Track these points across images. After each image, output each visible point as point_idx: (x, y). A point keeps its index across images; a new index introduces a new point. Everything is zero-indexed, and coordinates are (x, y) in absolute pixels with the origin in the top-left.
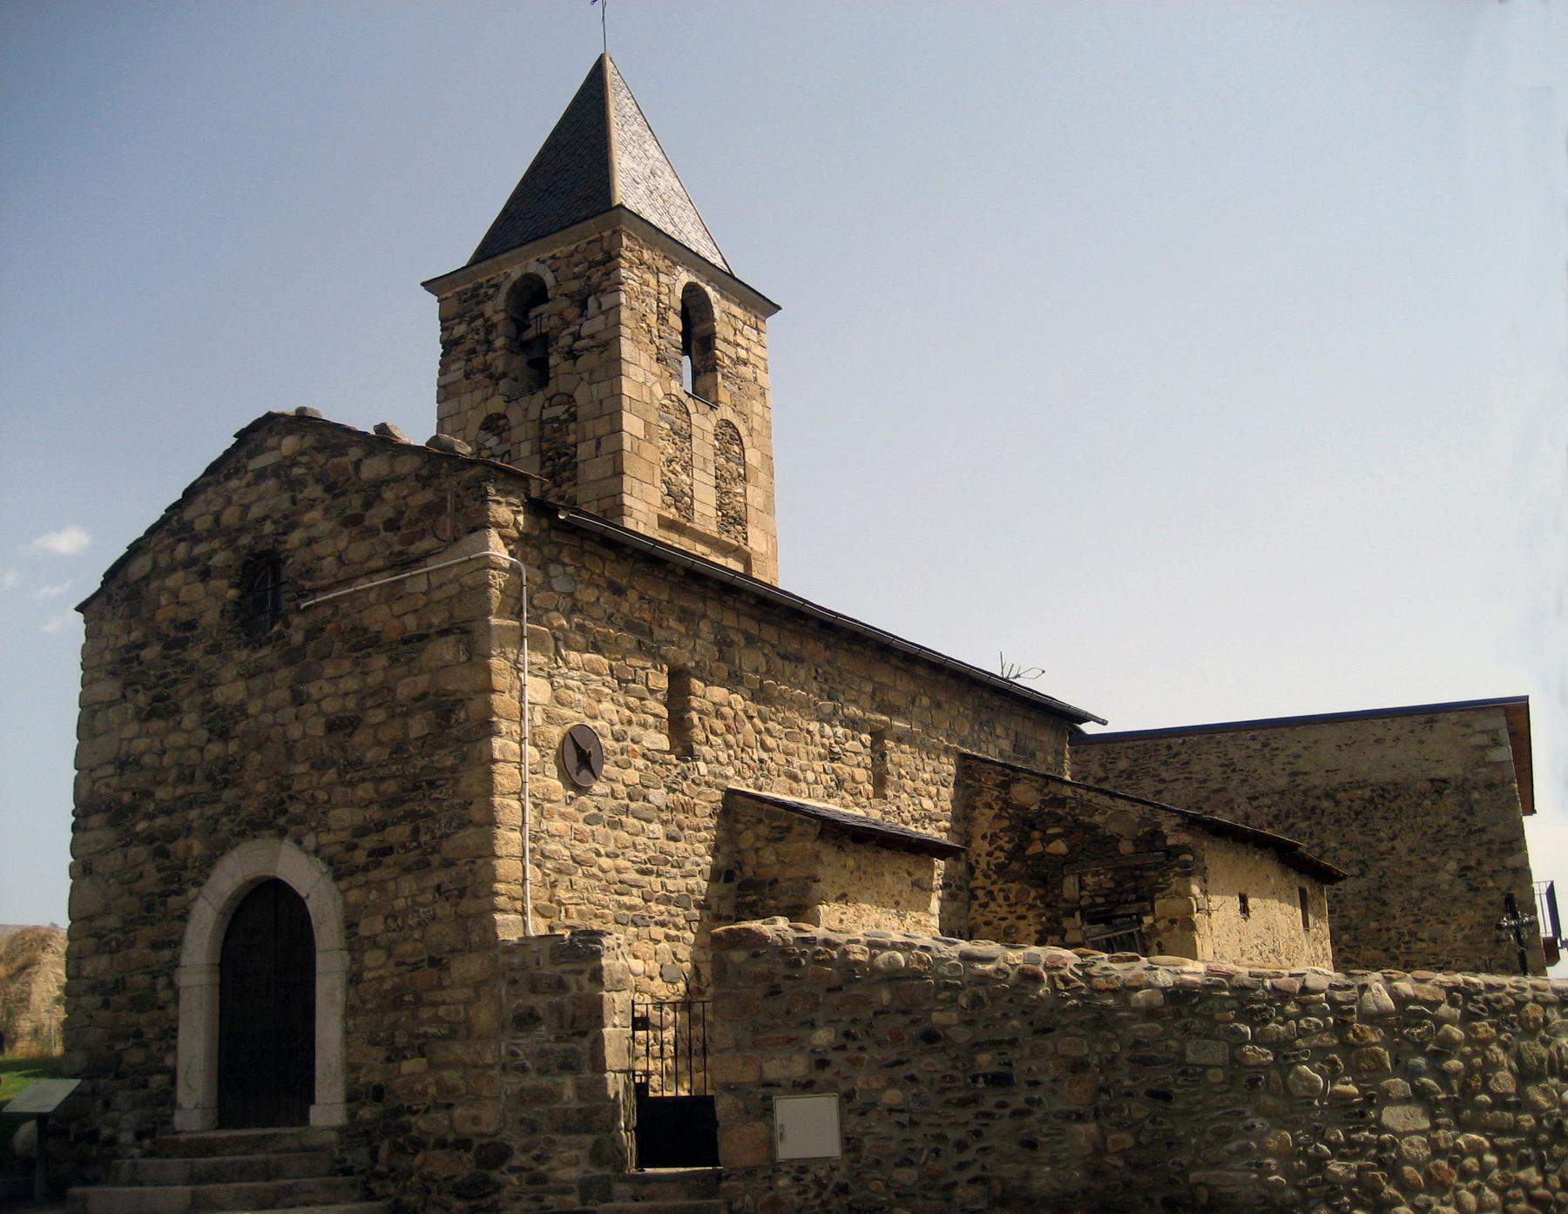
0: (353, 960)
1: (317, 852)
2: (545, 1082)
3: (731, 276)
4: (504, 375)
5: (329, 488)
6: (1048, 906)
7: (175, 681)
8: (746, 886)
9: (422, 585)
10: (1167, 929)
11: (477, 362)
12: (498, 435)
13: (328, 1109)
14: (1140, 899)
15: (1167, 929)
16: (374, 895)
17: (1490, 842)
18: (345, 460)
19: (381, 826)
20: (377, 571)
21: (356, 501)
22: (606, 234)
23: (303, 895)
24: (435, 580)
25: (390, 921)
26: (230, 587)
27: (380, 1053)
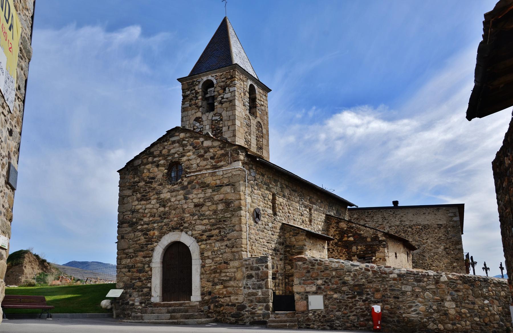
0: (203, 262)
1: (192, 236)
2: (254, 291)
3: (259, 81)
4: (201, 106)
5: (194, 148)
6: (348, 253)
7: (149, 192)
8: (287, 246)
9: (221, 173)
10: (379, 261)
11: (193, 102)
12: (200, 123)
13: (196, 297)
14: (372, 253)
15: (379, 261)
16: (208, 246)
17: (453, 242)
18: (199, 141)
19: (210, 230)
20: (208, 169)
21: (202, 152)
22: (231, 71)
23: (188, 246)
24: (225, 172)
25: (213, 253)
26: (165, 169)
27: (210, 284)
